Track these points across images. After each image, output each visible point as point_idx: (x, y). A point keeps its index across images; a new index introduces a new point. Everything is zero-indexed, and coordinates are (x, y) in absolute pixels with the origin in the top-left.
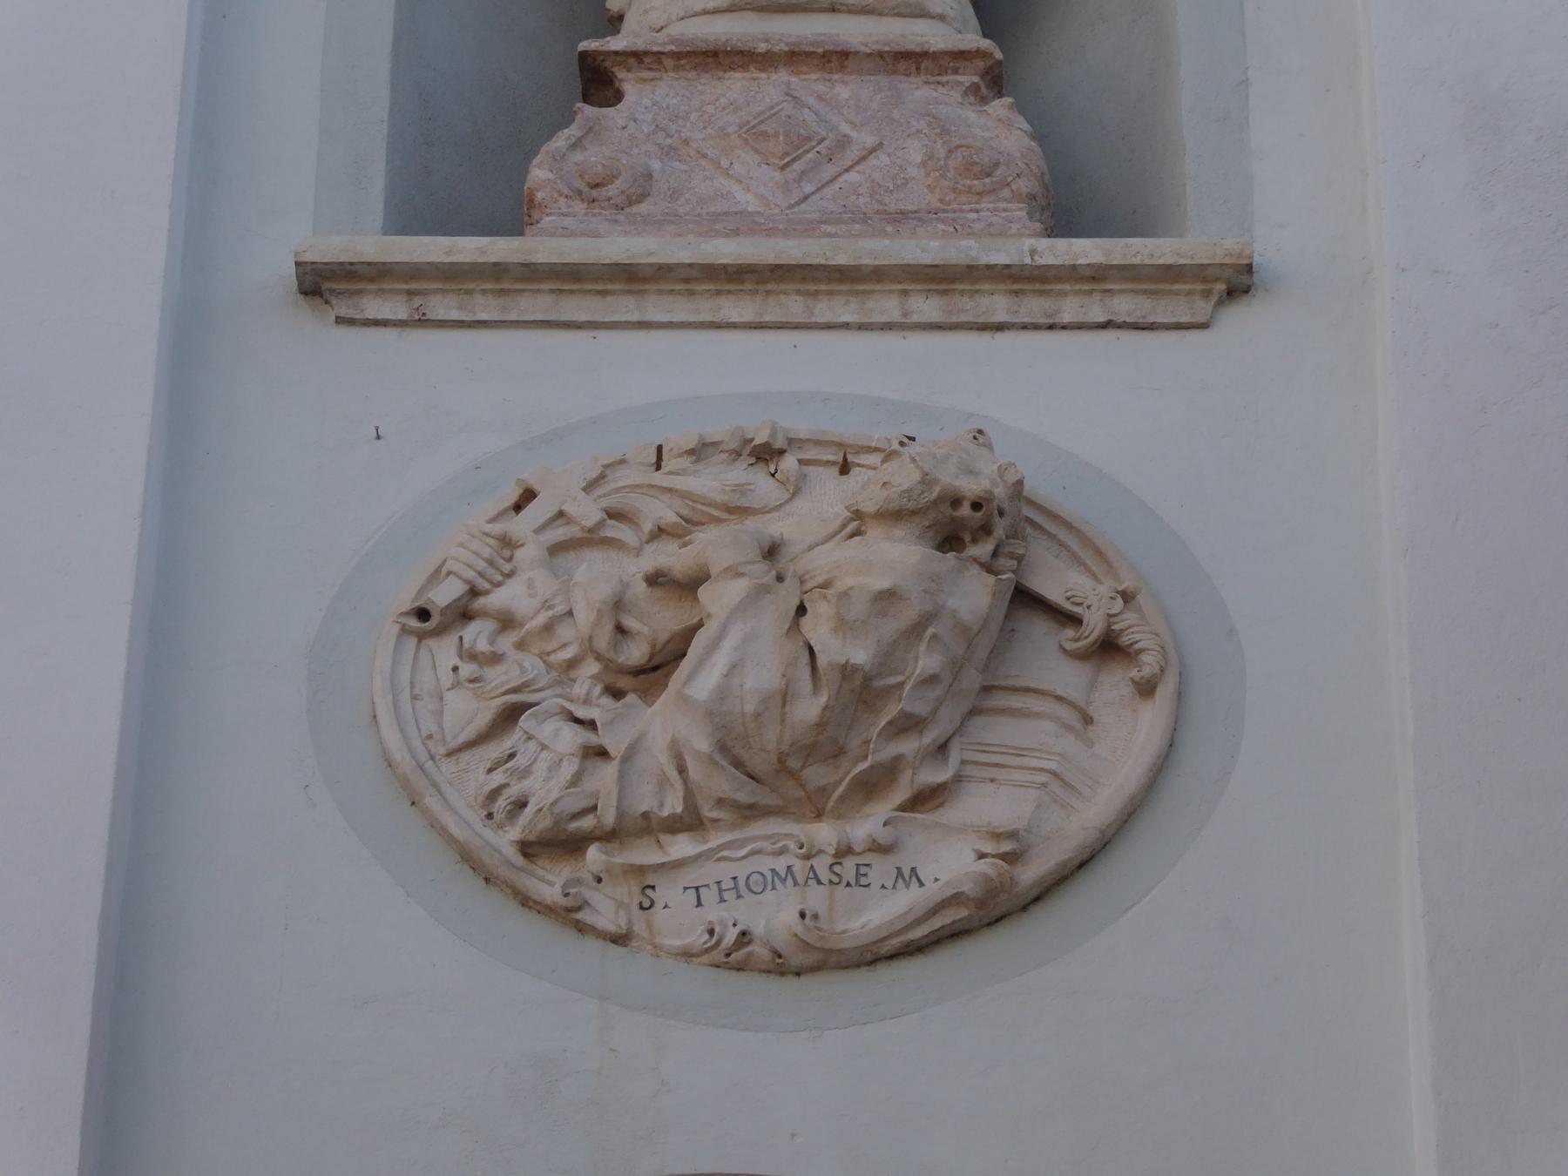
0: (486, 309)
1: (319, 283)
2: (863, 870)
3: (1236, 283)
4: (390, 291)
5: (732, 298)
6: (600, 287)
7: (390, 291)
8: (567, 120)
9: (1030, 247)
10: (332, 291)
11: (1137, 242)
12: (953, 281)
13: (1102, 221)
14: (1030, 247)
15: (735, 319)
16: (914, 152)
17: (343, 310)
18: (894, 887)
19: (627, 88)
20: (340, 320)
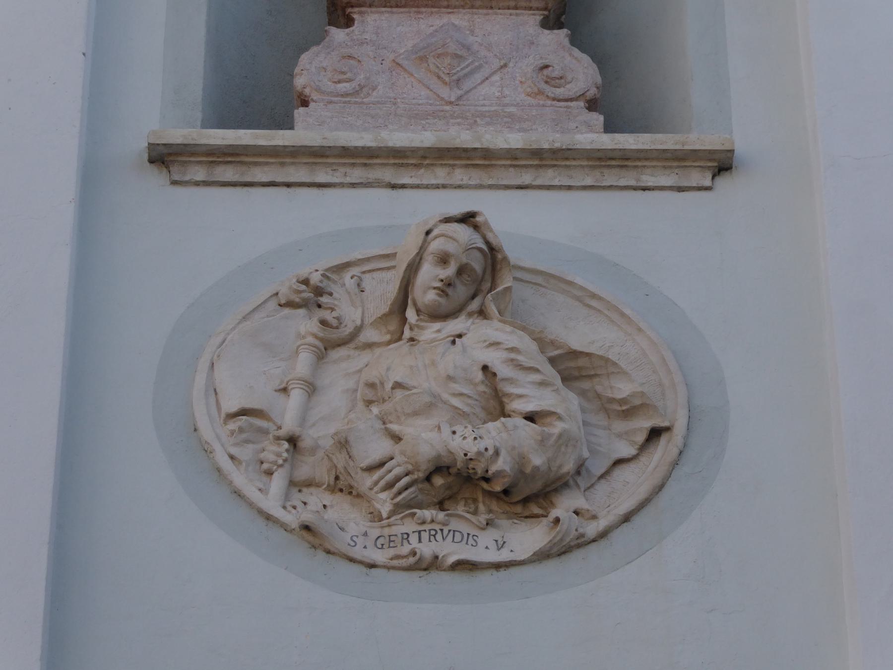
0: (357, 174)
1: (163, 157)
2: (392, 538)
3: (722, 165)
4: (300, 163)
5: (648, 171)
6: (352, 161)
7: (300, 163)
8: (319, 38)
9: (590, 135)
10: (172, 161)
11: (659, 136)
12: (372, 157)
13: (633, 123)
14: (590, 135)
15: (650, 184)
16: (517, 73)
17: (176, 177)
18: (402, 545)
19: (355, 16)
20: (174, 183)
